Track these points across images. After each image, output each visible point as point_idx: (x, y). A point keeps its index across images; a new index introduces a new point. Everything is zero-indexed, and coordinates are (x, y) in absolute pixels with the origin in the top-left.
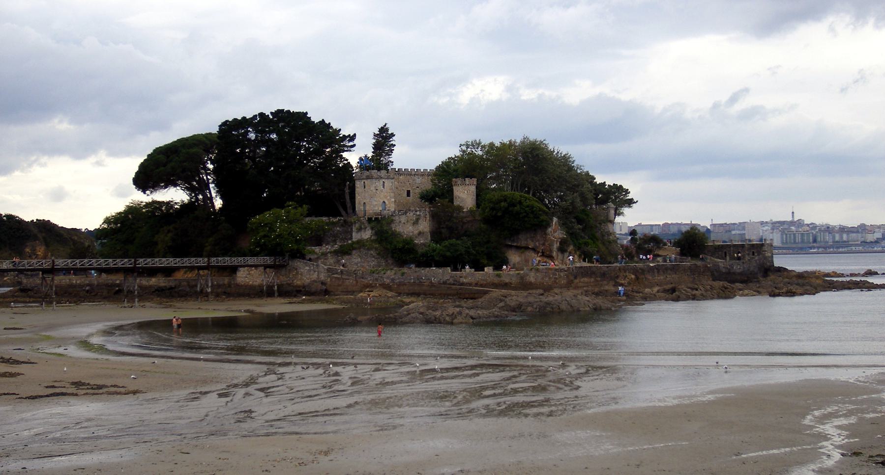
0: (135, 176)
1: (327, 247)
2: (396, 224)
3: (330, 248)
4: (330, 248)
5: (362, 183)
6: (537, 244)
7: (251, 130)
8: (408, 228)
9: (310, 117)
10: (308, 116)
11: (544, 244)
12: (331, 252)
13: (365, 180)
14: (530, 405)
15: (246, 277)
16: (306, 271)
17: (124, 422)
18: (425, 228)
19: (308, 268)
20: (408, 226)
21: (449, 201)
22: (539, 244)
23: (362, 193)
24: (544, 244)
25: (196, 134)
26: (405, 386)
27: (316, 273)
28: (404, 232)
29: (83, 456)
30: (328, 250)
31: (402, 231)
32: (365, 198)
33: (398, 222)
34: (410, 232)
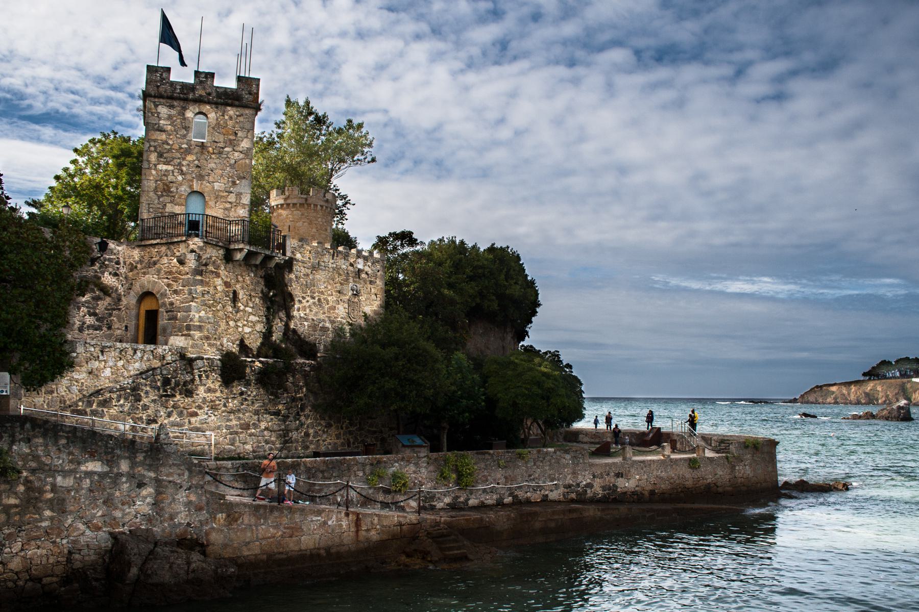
16: (87, 483)
19: (94, 466)
27: (148, 491)
32: (201, 177)
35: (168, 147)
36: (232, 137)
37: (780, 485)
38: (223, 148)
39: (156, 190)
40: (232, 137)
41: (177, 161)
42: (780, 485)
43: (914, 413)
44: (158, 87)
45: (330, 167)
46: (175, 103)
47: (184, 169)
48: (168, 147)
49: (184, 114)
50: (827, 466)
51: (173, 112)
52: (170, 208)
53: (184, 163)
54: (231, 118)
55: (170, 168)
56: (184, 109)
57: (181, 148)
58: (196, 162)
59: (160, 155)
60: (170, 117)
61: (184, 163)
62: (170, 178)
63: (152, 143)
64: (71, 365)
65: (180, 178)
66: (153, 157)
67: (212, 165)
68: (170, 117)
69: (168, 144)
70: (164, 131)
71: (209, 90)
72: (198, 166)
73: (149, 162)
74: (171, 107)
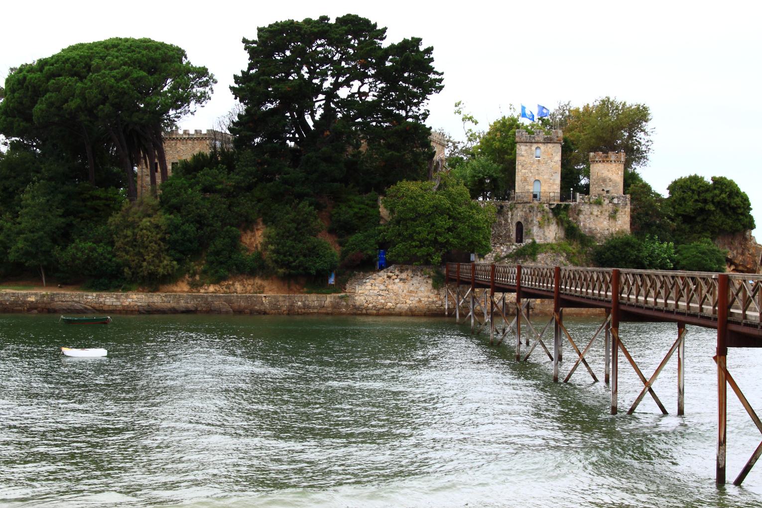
0: (400, 44)
1: (502, 248)
2: (586, 216)
3: (505, 250)
4: (505, 250)
6: (735, 252)
7: (251, 72)
8: (602, 223)
10: (378, 28)
11: (743, 254)
12: (508, 256)
13: (540, 145)
14: (44, 495)
15: (379, 295)
17: (312, 460)
18: (625, 224)
20: (602, 220)
21: (629, 186)
22: (737, 253)
23: (533, 164)
24: (743, 254)
25: (299, 18)
26: (32, 479)
28: (596, 229)
29: (366, 487)
30: (503, 253)
31: (593, 226)
32: (539, 174)
33: (588, 213)
34: (604, 230)
39: (521, 181)
41: (529, 168)
46: (528, 144)
47: (532, 171)
51: (527, 148)
52: (527, 187)
55: (527, 171)
56: (531, 146)
59: (523, 166)
60: (526, 150)
62: (527, 175)
65: (530, 175)
68: (526, 150)
74: (526, 146)
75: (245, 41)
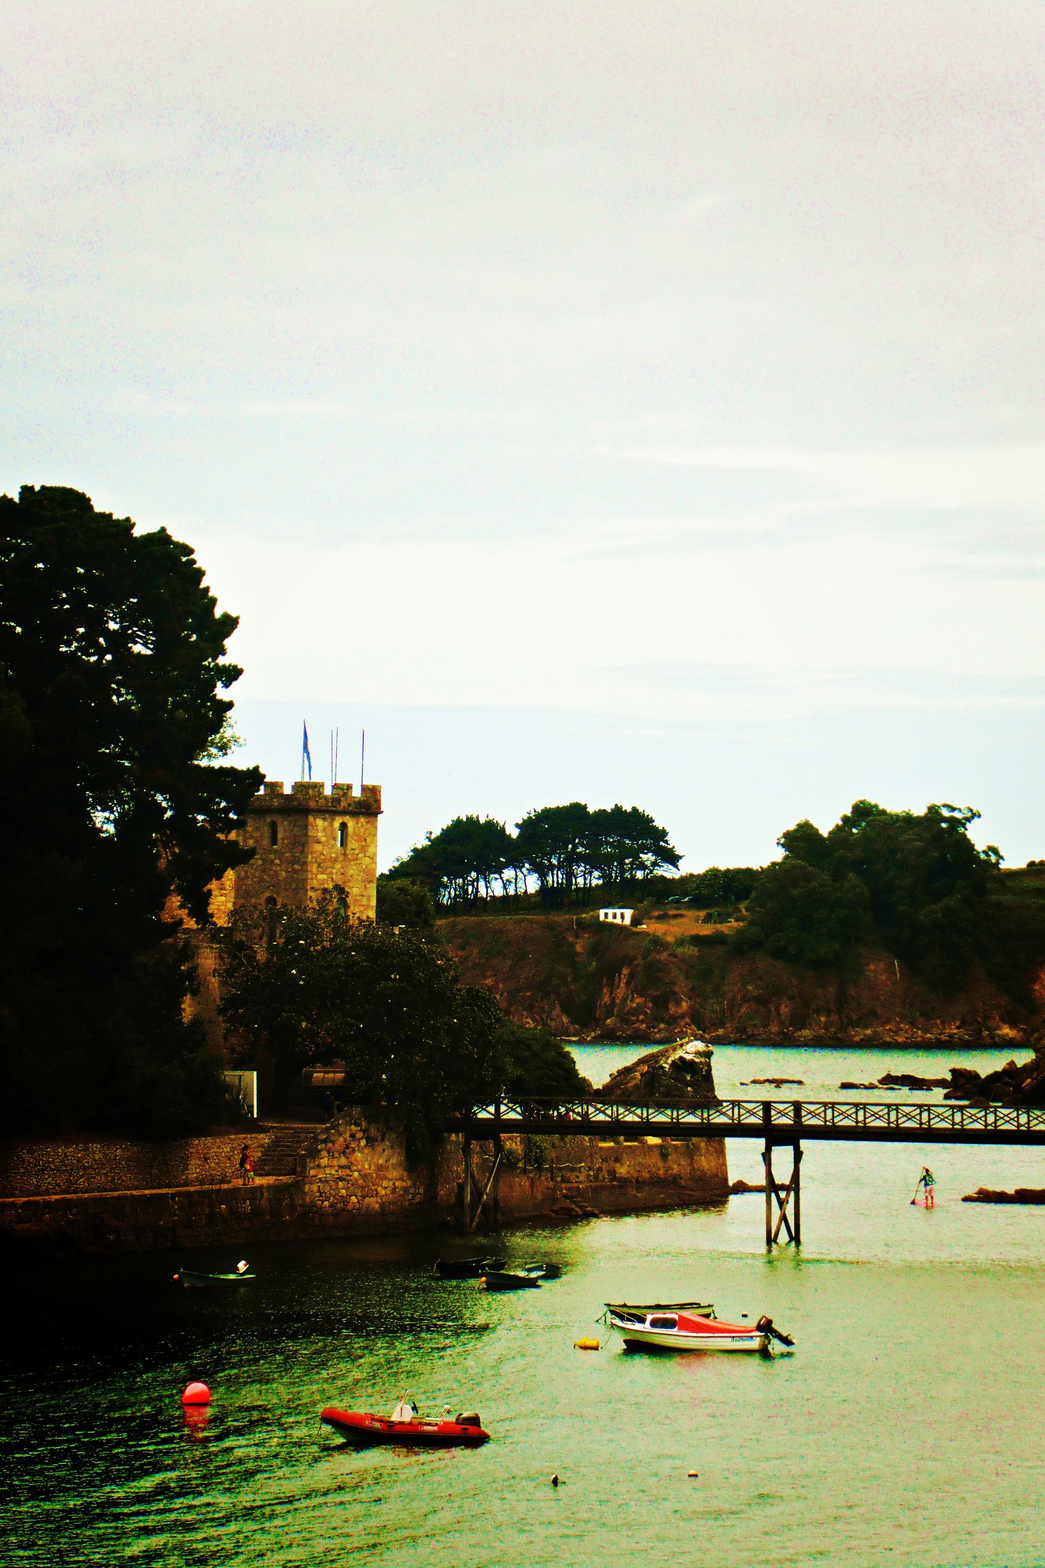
5: (337, 824)
9: (163, 530)
35: (323, 857)
36: (363, 844)
37: (731, 1184)
38: (358, 854)
40: (363, 844)
42: (212, 760)
43: (355, 1507)
44: (317, 801)
45: (1005, 1408)
47: (334, 877)
48: (323, 857)
49: (332, 826)
50: (231, 1536)
51: (326, 824)
53: (334, 871)
54: (362, 826)
56: (333, 820)
57: (331, 857)
58: (341, 870)
59: (319, 866)
60: (324, 829)
61: (334, 871)
63: (315, 855)
64: (196, 995)
66: (314, 869)
67: (351, 872)
69: (323, 855)
70: (319, 843)
71: (349, 801)
72: (343, 874)
73: (311, 871)
75: (975, 815)
